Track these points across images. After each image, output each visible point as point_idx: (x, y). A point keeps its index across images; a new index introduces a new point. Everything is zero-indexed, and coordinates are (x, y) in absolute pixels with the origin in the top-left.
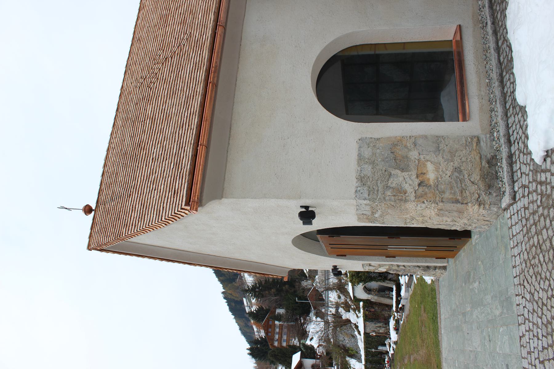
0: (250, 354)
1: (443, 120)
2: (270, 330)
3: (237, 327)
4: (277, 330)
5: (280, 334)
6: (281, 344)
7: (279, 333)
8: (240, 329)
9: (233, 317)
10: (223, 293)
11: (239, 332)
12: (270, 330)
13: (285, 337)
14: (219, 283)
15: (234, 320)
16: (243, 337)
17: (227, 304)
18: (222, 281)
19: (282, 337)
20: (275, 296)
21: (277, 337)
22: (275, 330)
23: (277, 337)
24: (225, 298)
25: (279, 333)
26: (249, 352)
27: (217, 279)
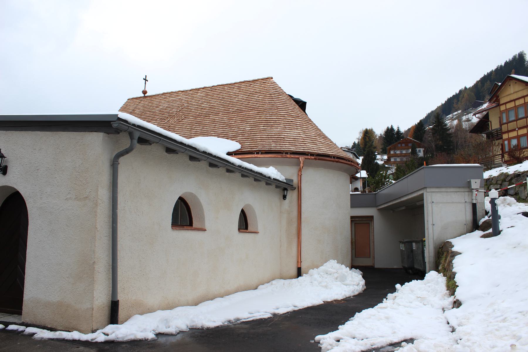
0: (388, 129)
1: (117, 324)
2: (403, 145)
3: (434, 108)
4: (404, 152)
5: (401, 155)
6: (392, 157)
7: (401, 153)
8: (432, 112)
9: (444, 102)
10: (465, 88)
11: (429, 111)
12: (403, 145)
13: (398, 159)
14: (475, 82)
15: (440, 105)
16: (425, 115)
17: (454, 94)
18: (476, 85)
19: (404, 156)
20: (436, 146)
21: (398, 152)
22: (404, 149)
23: (398, 152)
24: (460, 91)
25: (401, 153)
26: (390, 127)
27: (478, 79)
